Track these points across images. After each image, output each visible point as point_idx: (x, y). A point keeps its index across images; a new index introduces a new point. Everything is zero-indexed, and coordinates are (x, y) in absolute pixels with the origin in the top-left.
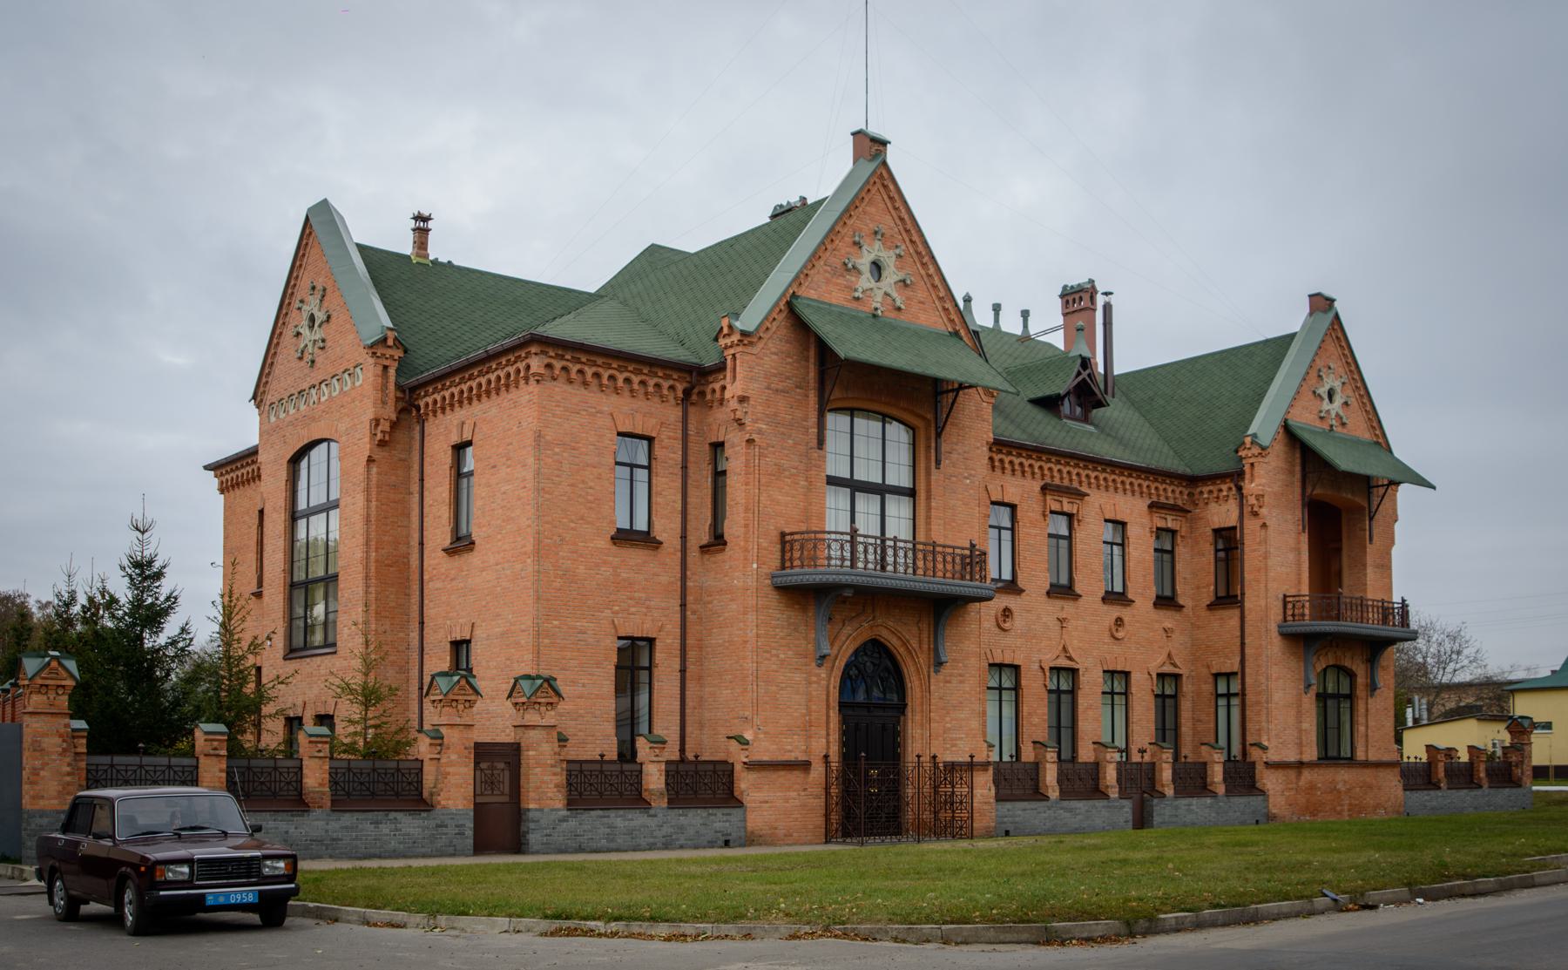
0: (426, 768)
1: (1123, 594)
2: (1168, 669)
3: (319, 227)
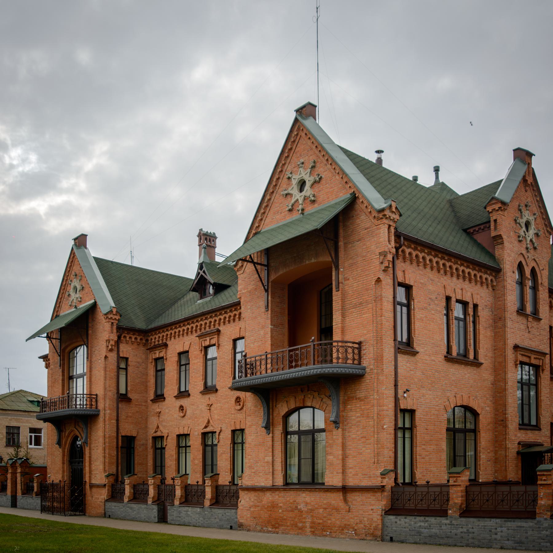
1: (126, 395)
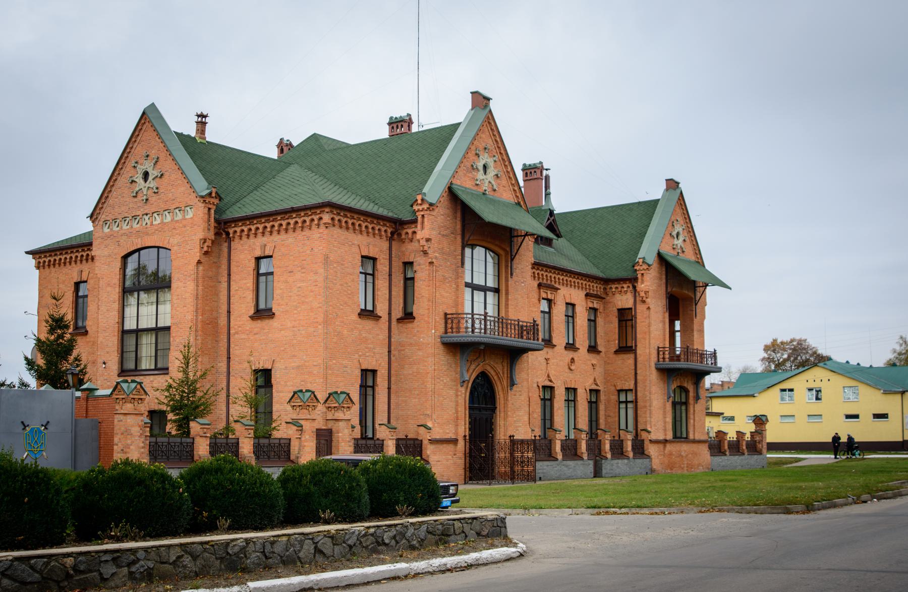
0: (292, 443)
1: (373, 311)
2: (548, 383)
3: (149, 120)
